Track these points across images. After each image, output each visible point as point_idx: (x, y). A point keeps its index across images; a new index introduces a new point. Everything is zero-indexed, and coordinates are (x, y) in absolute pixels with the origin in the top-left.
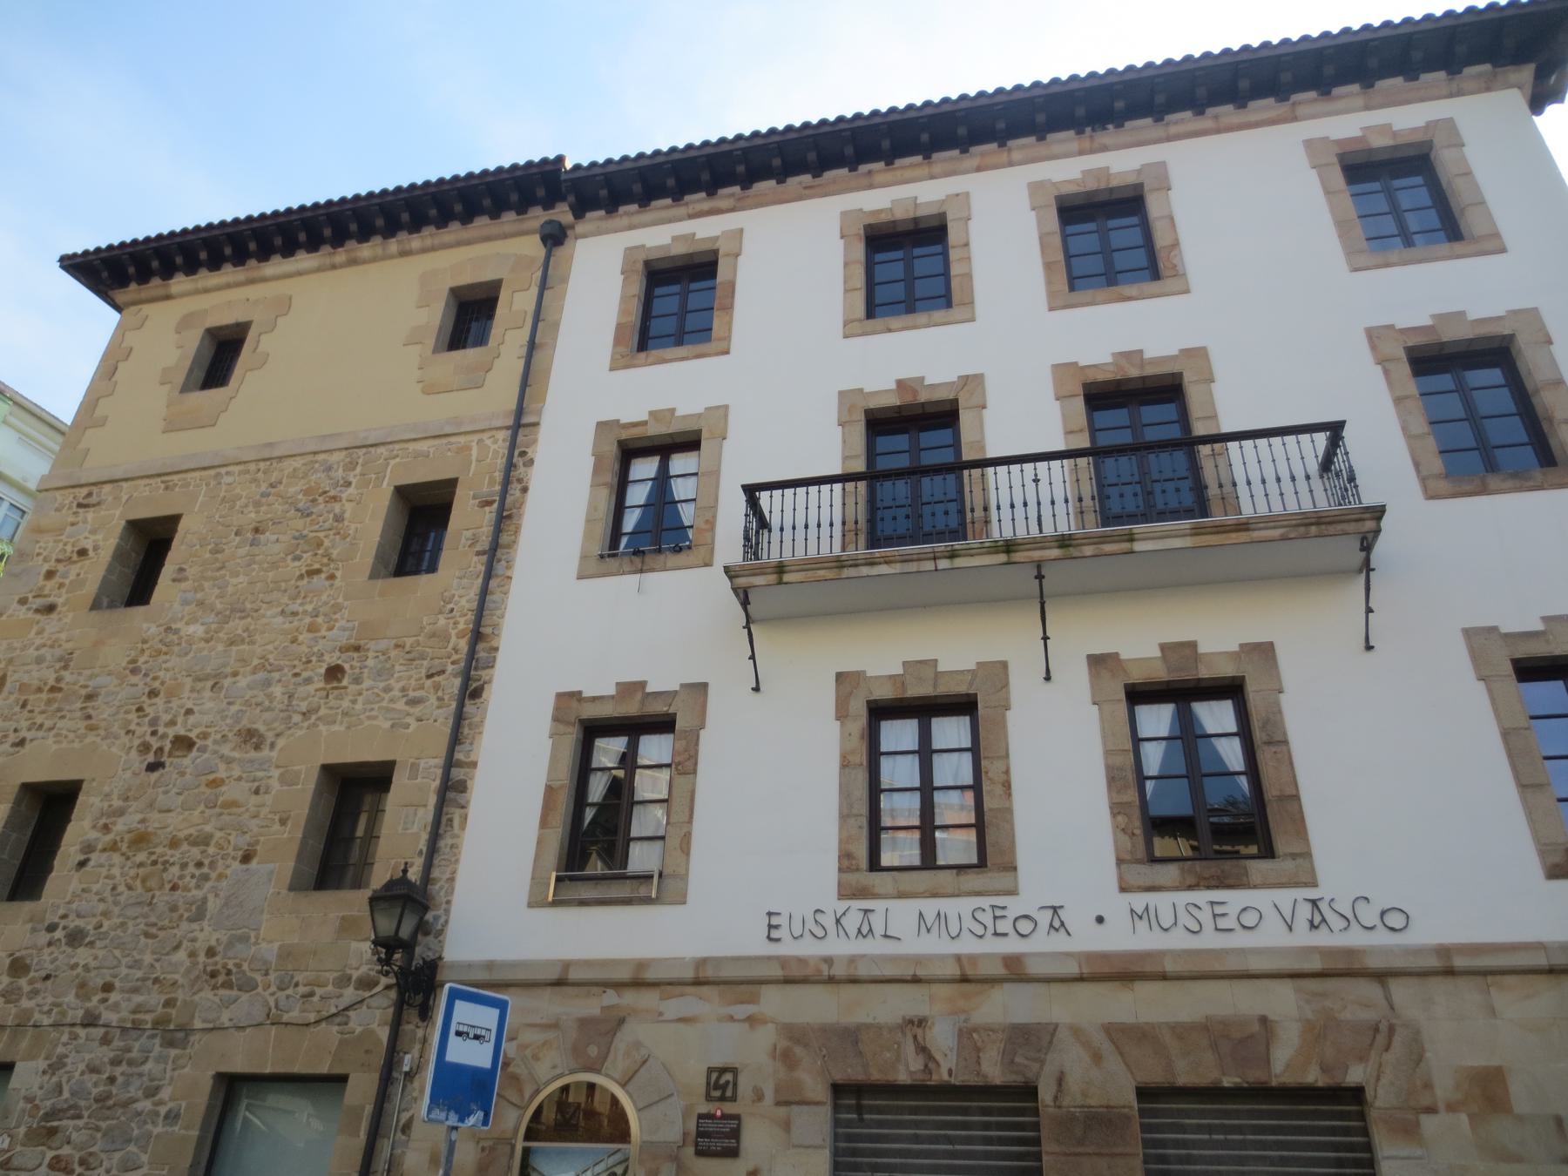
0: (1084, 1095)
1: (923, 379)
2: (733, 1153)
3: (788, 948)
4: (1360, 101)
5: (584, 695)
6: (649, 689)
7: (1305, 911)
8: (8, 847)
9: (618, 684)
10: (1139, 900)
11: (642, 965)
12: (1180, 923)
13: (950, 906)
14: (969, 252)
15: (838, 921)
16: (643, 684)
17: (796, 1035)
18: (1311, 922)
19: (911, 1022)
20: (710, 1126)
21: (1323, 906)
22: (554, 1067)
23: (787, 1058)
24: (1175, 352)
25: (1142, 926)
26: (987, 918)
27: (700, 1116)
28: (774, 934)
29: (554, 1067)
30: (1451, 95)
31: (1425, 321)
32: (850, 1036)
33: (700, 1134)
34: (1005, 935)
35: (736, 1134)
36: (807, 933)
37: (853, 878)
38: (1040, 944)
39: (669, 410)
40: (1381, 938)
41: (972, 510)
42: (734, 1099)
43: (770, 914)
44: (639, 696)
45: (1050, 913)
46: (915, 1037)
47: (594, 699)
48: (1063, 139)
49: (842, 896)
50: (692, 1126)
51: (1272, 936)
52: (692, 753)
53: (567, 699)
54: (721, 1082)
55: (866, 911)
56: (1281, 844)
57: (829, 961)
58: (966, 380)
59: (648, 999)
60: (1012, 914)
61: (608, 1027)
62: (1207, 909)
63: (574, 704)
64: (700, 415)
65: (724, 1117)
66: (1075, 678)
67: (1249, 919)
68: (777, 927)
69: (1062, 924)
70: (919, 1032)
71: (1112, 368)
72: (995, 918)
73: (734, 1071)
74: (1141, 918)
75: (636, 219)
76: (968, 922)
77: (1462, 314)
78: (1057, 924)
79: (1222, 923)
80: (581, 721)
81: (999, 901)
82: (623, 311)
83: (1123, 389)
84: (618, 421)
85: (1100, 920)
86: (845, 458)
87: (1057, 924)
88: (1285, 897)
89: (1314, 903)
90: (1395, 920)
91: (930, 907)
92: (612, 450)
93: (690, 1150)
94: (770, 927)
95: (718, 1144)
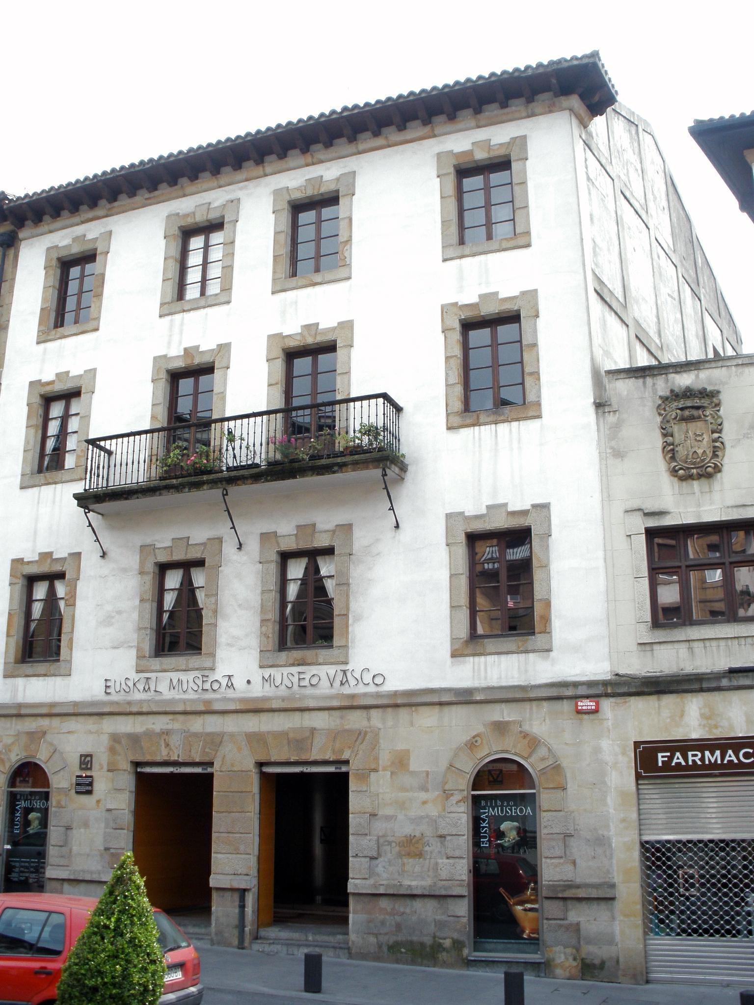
0: (232, 765)
1: (198, 347)
2: (89, 792)
3: (114, 697)
4: (473, 123)
5: (25, 560)
6: (55, 557)
7: (340, 676)
8: (615, 869)
9: (40, 554)
10: (267, 672)
11: (53, 705)
12: (283, 684)
13: (183, 676)
14: (233, 249)
15: (134, 684)
16: (51, 554)
17: (115, 738)
18: (341, 682)
19: (163, 733)
20: (81, 781)
21: (349, 674)
22: (18, 755)
23: (112, 750)
24: (336, 325)
25: (267, 685)
26: (199, 682)
27: (77, 776)
28: (108, 691)
29: (18, 755)
30: (528, 117)
31: (474, 299)
32: (134, 739)
33: (78, 784)
34: (207, 690)
35: (91, 784)
36: (122, 690)
37: (144, 662)
38: (220, 697)
39: (65, 372)
40: (372, 689)
41: (214, 452)
42: (90, 769)
43: (106, 680)
44: (49, 561)
45: (227, 679)
46: (165, 740)
47: (29, 563)
48: (295, 157)
49: (138, 671)
50: (74, 781)
51: (324, 689)
52: (73, 594)
53: (17, 562)
54: (86, 761)
55: (148, 678)
56: (336, 641)
57: (129, 703)
58: (221, 347)
59: (56, 721)
60: (211, 679)
61: (36, 737)
62: (297, 676)
63: (20, 566)
64: (81, 376)
65: (86, 777)
66: (253, 545)
67: (314, 681)
68: (109, 687)
69: (232, 684)
70: (167, 738)
71: (298, 338)
72: (203, 681)
73: (91, 756)
74: (267, 681)
75: (53, 226)
76: (191, 684)
77: (496, 294)
78: (230, 684)
79: (302, 684)
80: (24, 576)
81: (206, 673)
82: (44, 300)
83: (279, 435)
84: (40, 381)
85: (249, 682)
86: (153, 417)
87: (230, 684)
88: (331, 670)
89: (344, 672)
90: (379, 680)
91: (175, 676)
92: (37, 400)
93: (73, 791)
94: (106, 686)
95: (83, 789)
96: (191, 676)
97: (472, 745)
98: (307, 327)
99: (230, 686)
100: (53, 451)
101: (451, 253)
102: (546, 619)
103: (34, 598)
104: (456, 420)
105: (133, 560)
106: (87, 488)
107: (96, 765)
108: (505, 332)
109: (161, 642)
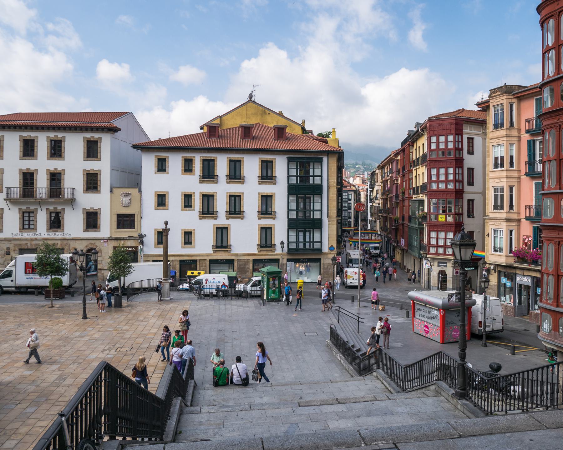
2: (9, 254)
10: (48, 233)
13: (30, 233)
88: (61, 233)
91: (28, 233)
96: (32, 233)
97: (86, 246)
98: (55, 169)
99: (40, 235)
100: (318, 135)
101: (85, 159)
102: (100, 227)
103: (431, 237)
104: (85, 192)
105: (17, 211)
106: (457, 156)
107: (10, 249)
108: (211, 163)
109: (302, 252)
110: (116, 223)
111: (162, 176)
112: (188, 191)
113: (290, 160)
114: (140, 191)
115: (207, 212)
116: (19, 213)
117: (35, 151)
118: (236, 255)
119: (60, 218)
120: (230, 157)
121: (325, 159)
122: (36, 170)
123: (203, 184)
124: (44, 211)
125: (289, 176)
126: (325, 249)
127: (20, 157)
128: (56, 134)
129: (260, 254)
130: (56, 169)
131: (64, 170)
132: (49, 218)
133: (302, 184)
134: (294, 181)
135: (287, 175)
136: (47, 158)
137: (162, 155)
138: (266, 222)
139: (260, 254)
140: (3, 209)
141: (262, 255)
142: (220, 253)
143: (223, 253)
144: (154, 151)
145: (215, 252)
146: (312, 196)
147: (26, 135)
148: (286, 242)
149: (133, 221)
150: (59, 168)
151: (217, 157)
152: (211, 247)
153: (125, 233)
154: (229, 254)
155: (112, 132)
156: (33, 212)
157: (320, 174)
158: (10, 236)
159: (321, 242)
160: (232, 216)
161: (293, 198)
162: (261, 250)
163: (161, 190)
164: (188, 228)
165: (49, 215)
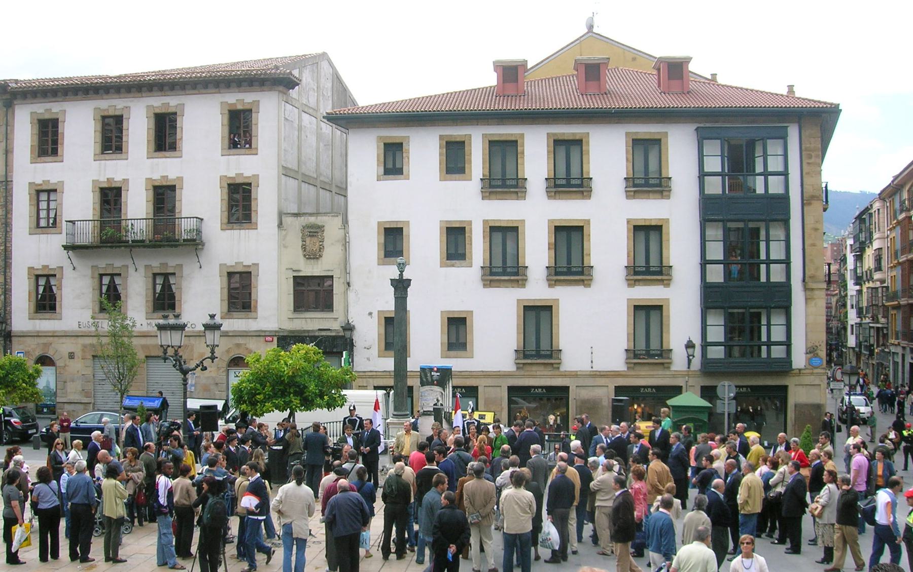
10: (149, 321)
97: (228, 351)
98: (163, 177)
102: (256, 307)
104: (225, 227)
105: (89, 272)
110: (292, 296)
111: (393, 185)
112: (456, 217)
113: (702, 137)
114: (345, 222)
115: (500, 270)
116: (93, 278)
117: (124, 139)
118: (575, 375)
119: (173, 287)
120: (554, 134)
121: (793, 133)
122: (126, 181)
123: (633, 201)
124: (142, 270)
125: (703, 175)
126: (799, 359)
127: (95, 155)
128: (48, 106)
129: (630, 373)
130: (165, 177)
131: (180, 179)
132: (150, 286)
133: (733, 194)
134: (715, 186)
135: (695, 172)
136: (148, 152)
137: (395, 134)
138: (649, 293)
139: (632, 373)
140: (62, 267)
141: (638, 376)
142: (644, 371)
143: (541, 371)
144: (609, 122)
145: (522, 368)
146: (762, 226)
147: (41, 111)
148: (697, 341)
149: (330, 292)
150: (247, 173)
151: (522, 135)
152: (511, 356)
153: (314, 322)
154: (557, 373)
155: (281, 88)
156: (120, 275)
157: (780, 168)
158: (75, 327)
159: (788, 344)
160: (562, 278)
161: (715, 232)
162: (635, 364)
163: (392, 217)
164: (457, 306)
165: (150, 280)
